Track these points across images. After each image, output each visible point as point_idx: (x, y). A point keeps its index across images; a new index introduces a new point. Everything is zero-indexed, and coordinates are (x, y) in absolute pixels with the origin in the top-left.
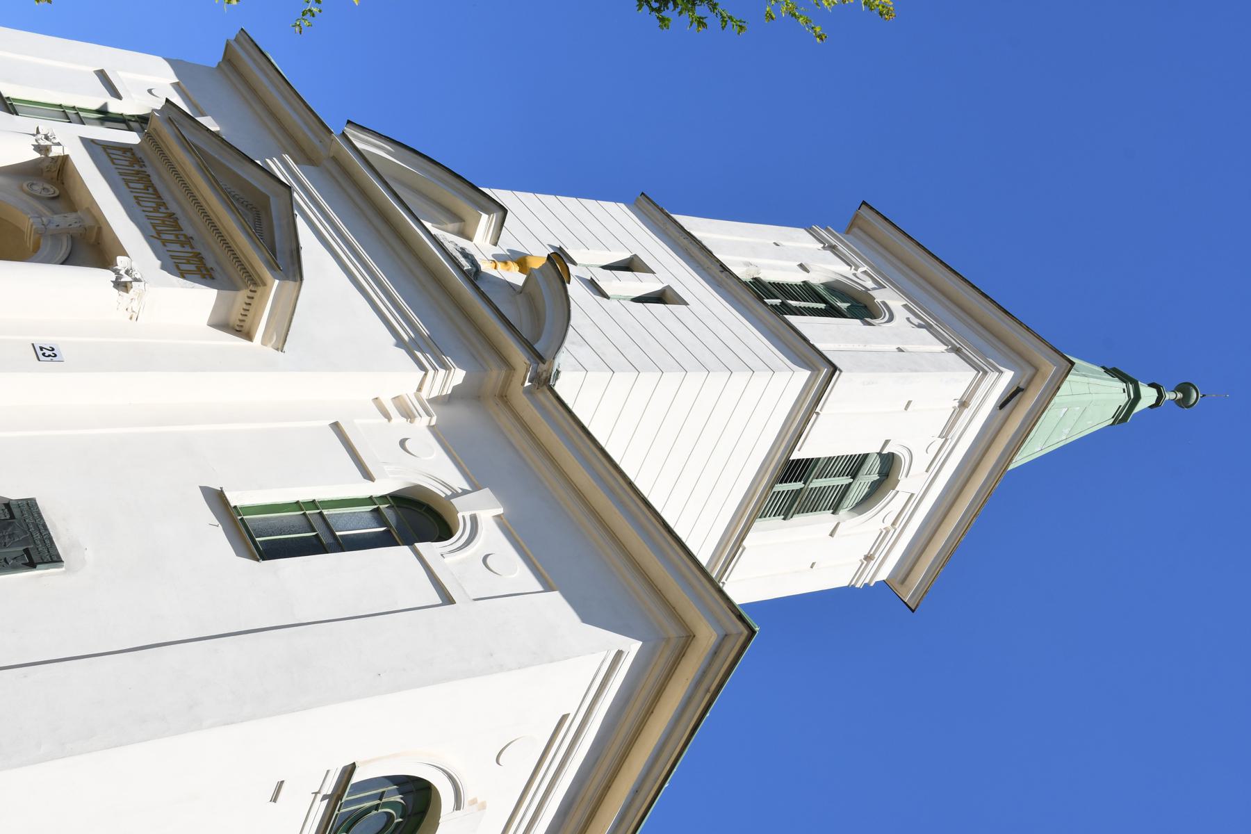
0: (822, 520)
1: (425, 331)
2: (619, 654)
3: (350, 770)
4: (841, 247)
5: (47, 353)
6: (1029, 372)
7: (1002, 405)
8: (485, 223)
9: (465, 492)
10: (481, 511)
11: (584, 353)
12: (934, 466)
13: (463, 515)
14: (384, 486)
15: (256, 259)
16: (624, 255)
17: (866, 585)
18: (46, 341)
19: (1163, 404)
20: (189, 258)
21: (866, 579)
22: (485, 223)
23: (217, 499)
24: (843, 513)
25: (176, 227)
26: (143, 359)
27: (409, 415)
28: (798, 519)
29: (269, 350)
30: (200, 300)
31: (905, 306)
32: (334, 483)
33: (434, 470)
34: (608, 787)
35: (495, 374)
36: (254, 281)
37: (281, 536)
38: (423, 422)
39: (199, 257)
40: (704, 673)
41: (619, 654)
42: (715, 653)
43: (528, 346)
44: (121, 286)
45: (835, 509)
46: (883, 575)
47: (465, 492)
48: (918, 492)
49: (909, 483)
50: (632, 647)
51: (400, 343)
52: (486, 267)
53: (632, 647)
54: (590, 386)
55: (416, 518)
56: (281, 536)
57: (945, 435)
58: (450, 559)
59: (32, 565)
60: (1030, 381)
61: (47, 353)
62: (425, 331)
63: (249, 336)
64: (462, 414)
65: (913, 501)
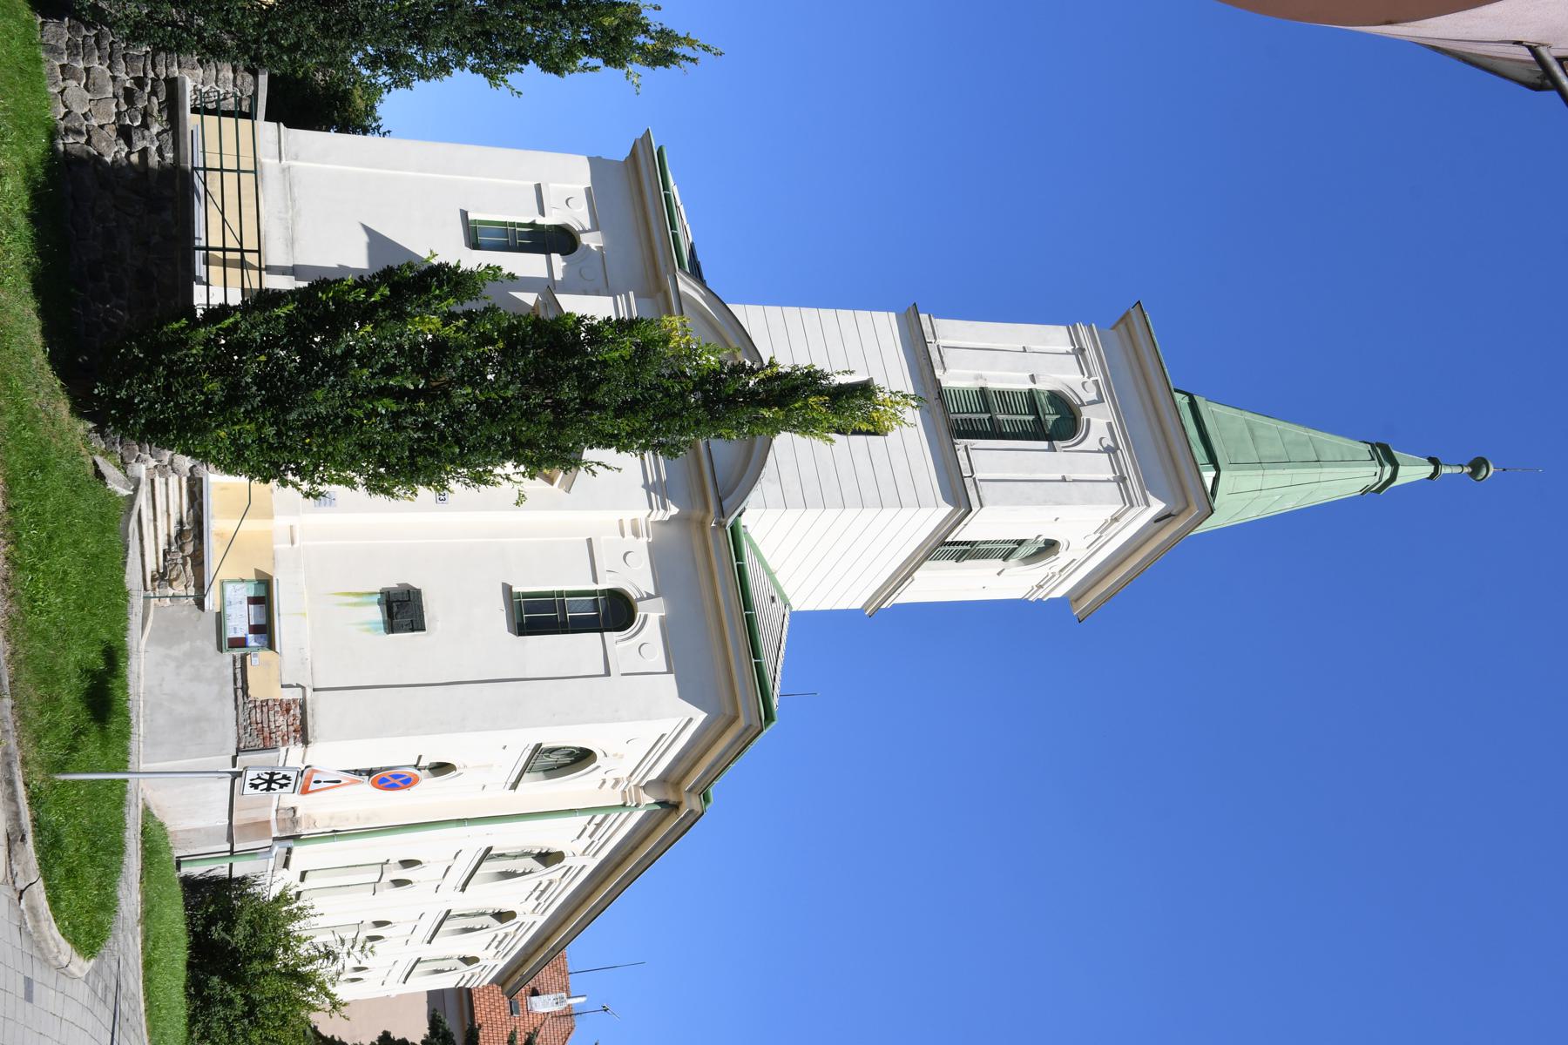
1: (664, 477)
2: (691, 720)
4: (1091, 353)
6: (1180, 506)
7: (1157, 520)
9: (650, 597)
13: (640, 615)
17: (1039, 601)
19: (1437, 479)
21: (1040, 594)
24: (1011, 561)
27: (636, 534)
28: (968, 562)
29: (562, 491)
31: (1110, 425)
33: (636, 578)
34: (701, 757)
35: (698, 513)
38: (644, 540)
40: (741, 735)
41: (691, 720)
42: (746, 729)
43: (720, 501)
44: (662, 57)
45: (1005, 559)
46: (1059, 593)
47: (650, 597)
49: (1063, 557)
50: (700, 716)
51: (646, 486)
53: (700, 716)
55: (614, 612)
56: (537, 616)
58: (621, 645)
59: (413, 630)
62: (664, 477)
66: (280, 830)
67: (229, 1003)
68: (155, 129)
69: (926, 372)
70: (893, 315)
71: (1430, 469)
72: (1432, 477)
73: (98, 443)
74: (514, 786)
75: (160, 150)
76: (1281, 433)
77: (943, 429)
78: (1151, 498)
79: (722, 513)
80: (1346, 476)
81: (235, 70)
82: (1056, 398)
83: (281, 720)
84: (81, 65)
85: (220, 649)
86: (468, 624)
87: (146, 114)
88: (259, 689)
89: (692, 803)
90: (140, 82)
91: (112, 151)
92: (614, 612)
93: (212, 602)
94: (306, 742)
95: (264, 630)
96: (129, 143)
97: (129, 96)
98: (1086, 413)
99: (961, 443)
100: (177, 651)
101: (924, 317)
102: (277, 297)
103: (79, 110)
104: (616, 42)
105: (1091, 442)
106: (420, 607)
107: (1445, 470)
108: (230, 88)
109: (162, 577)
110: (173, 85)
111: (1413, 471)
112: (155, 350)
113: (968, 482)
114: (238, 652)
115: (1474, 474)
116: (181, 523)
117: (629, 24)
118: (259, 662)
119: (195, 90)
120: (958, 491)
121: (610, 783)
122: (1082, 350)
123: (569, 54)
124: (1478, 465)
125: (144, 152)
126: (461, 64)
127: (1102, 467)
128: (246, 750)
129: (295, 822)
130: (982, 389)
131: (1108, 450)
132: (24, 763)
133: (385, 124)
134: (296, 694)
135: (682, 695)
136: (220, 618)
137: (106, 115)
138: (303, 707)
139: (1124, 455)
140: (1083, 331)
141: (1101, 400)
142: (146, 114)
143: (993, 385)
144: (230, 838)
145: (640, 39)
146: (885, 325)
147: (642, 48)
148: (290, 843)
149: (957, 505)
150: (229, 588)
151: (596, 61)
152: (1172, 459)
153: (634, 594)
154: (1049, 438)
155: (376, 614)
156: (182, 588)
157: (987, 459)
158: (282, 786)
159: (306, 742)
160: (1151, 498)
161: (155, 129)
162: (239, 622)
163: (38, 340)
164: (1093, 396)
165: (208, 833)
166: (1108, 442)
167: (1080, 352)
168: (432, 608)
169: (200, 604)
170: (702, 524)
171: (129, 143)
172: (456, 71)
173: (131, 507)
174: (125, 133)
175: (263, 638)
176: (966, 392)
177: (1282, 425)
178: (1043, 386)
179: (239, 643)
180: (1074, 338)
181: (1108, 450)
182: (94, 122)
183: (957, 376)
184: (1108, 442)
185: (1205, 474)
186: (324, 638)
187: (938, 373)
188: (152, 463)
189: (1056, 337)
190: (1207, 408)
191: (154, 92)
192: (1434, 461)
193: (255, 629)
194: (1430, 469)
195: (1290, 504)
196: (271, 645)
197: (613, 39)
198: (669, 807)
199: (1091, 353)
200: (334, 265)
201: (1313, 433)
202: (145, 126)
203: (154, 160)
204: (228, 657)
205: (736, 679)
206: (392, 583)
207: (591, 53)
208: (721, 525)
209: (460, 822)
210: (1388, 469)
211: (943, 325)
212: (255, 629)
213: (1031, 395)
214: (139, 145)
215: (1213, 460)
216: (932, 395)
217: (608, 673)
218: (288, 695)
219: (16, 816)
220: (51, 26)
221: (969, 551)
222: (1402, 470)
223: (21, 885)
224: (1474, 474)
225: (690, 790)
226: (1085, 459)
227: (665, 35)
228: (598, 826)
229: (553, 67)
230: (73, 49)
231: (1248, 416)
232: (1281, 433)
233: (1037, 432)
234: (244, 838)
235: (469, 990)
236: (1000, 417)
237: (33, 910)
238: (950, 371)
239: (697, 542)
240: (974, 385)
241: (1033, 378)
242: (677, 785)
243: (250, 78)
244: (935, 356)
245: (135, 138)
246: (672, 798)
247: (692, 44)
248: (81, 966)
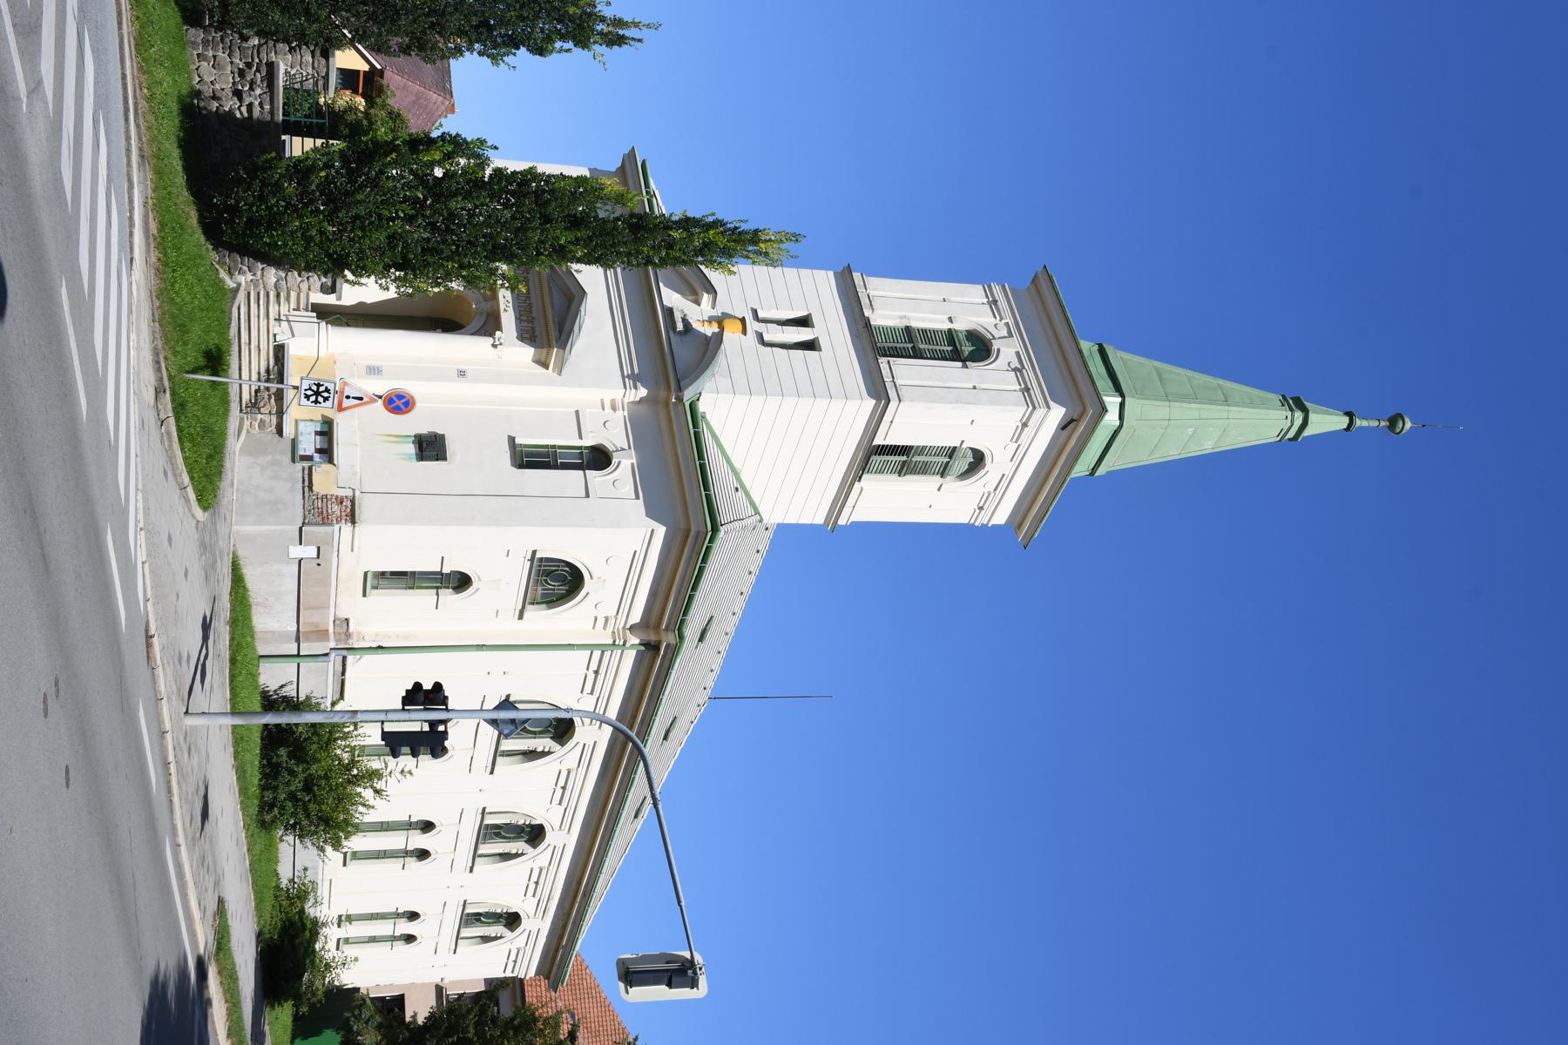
0: (932, 481)
3: (534, 552)
4: (1002, 303)
5: (462, 374)
6: (1079, 410)
8: (706, 298)
10: (1008, 350)
12: (1018, 458)
18: (462, 367)
19: (1353, 429)
20: (528, 335)
21: (983, 519)
22: (706, 298)
23: (512, 440)
25: (530, 312)
26: (498, 377)
27: (614, 409)
30: (528, 352)
31: (1018, 353)
32: (564, 438)
33: (614, 435)
35: (663, 394)
36: (550, 346)
37: (530, 459)
38: (620, 413)
39: (533, 329)
43: (678, 381)
44: (616, 40)
52: (695, 325)
54: (720, 404)
55: (598, 458)
56: (530, 459)
57: (1016, 438)
60: (1081, 415)
61: (462, 374)
63: (546, 367)
64: (643, 409)
66: (337, 640)
67: (292, 773)
68: (258, 91)
69: (857, 309)
70: (831, 273)
71: (1346, 420)
72: (1348, 429)
74: (521, 617)
75: (261, 104)
76: (1189, 378)
77: (869, 348)
78: (1052, 404)
79: (680, 389)
81: (313, 53)
82: (973, 336)
83: (336, 508)
84: (211, 53)
85: (293, 461)
86: (478, 459)
87: (252, 83)
88: (318, 487)
89: (668, 639)
90: (249, 65)
91: (229, 104)
92: (598, 458)
94: (353, 522)
95: (327, 452)
96: (240, 99)
97: (242, 73)
98: (996, 345)
100: (261, 460)
101: (857, 276)
103: (208, 79)
104: (583, 29)
105: (1001, 363)
106: (444, 446)
107: (1359, 423)
108: (310, 70)
109: (254, 405)
110: (271, 67)
111: (1326, 422)
112: (253, 171)
113: (889, 386)
114: (306, 464)
116: (268, 371)
117: (590, 15)
118: (322, 473)
119: (286, 72)
120: (879, 390)
122: (995, 302)
123: (549, 39)
125: (250, 106)
128: (309, 524)
129: (348, 635)
130: (908, 328)
131: (1015, 370)
132: (166, 358)
133: (531, 612)
134: (349, 493)
135: (648, 515)
136: (294, 443)
137: (225, 83)
138: (353, 502)
139: (1029, 373)
140: (997, 290)
141: (1010, 335)
142: (252, 83)
143: (915, 324)
144: (298, 640)
145: (599, 27)
146: (825, 281)
148: (345, 653)
150: (301, 425)
151: (570, 45)
152: (1074, 380)
153: (611, 448)
154: (964, 361)
155: (411, 449)
156: (267, 416)
157: (904, 371)
158: (326, 399)
159: (353, 522)
160: (1052, 404)
161: (258, 91)
162: (308, 445)
163: (180, 168)
164: (1004, 332)
166: (1015, 364)
167: (993, 303)
168: (451, 447)
170: (667, 403)
171: (240, 99)
172: (467, 54)
173: (234, 298)
174: (238, 94)
175: (325, 457)
176: (893, 330)
177: (1190, 373)
178: (961, 326)
180: (989, 292)
181: (1015, 370)
182: (217, 86)
184: (1015, 364)
186: (368, 450)
187: (867, 313)
189: (975, 293)
190: (1117, 357)
191: (258, 70)
192: (1350, 414)
193: (319, 451)
196: (331, 461)
197: (580, 26)
198: (651, 648)
199: (1002, 303)
201: (1221, 382)
202: (252, 89)
204: (299, 466)
205: (689, 500)
206: (424, 430)
207: (563, 38)
208: (680, 400)
209: (480, 647)
210: (1299, 416)
211: (872, 282)
212: (319, 451)
214: (247, 100)
215: (1118, 389)
216: (861, 328)
217: (587, 496)
218: (341, 493)
219: (161, 379)
220: (192, 31)
221: (905, 459)
222: (1312, 417)
223: (163, 416)
225: (667, 629)
226: (996, 375)
227: (619, 23)
228: (596, 672)
229: (540, 51)
231: (1157, 364)
232: (1189, 378)
233: (956, 355)
234: (308, 639)
235: (521, 980)
236: (922, 346)
237: (169, 433)
238: (879, 312)
239: (662, 416)
241: (950, 319)
243: (323, 61)
245: (235, 445)
246: (653, 638)
247: (636, 25)
248: (198, 512)
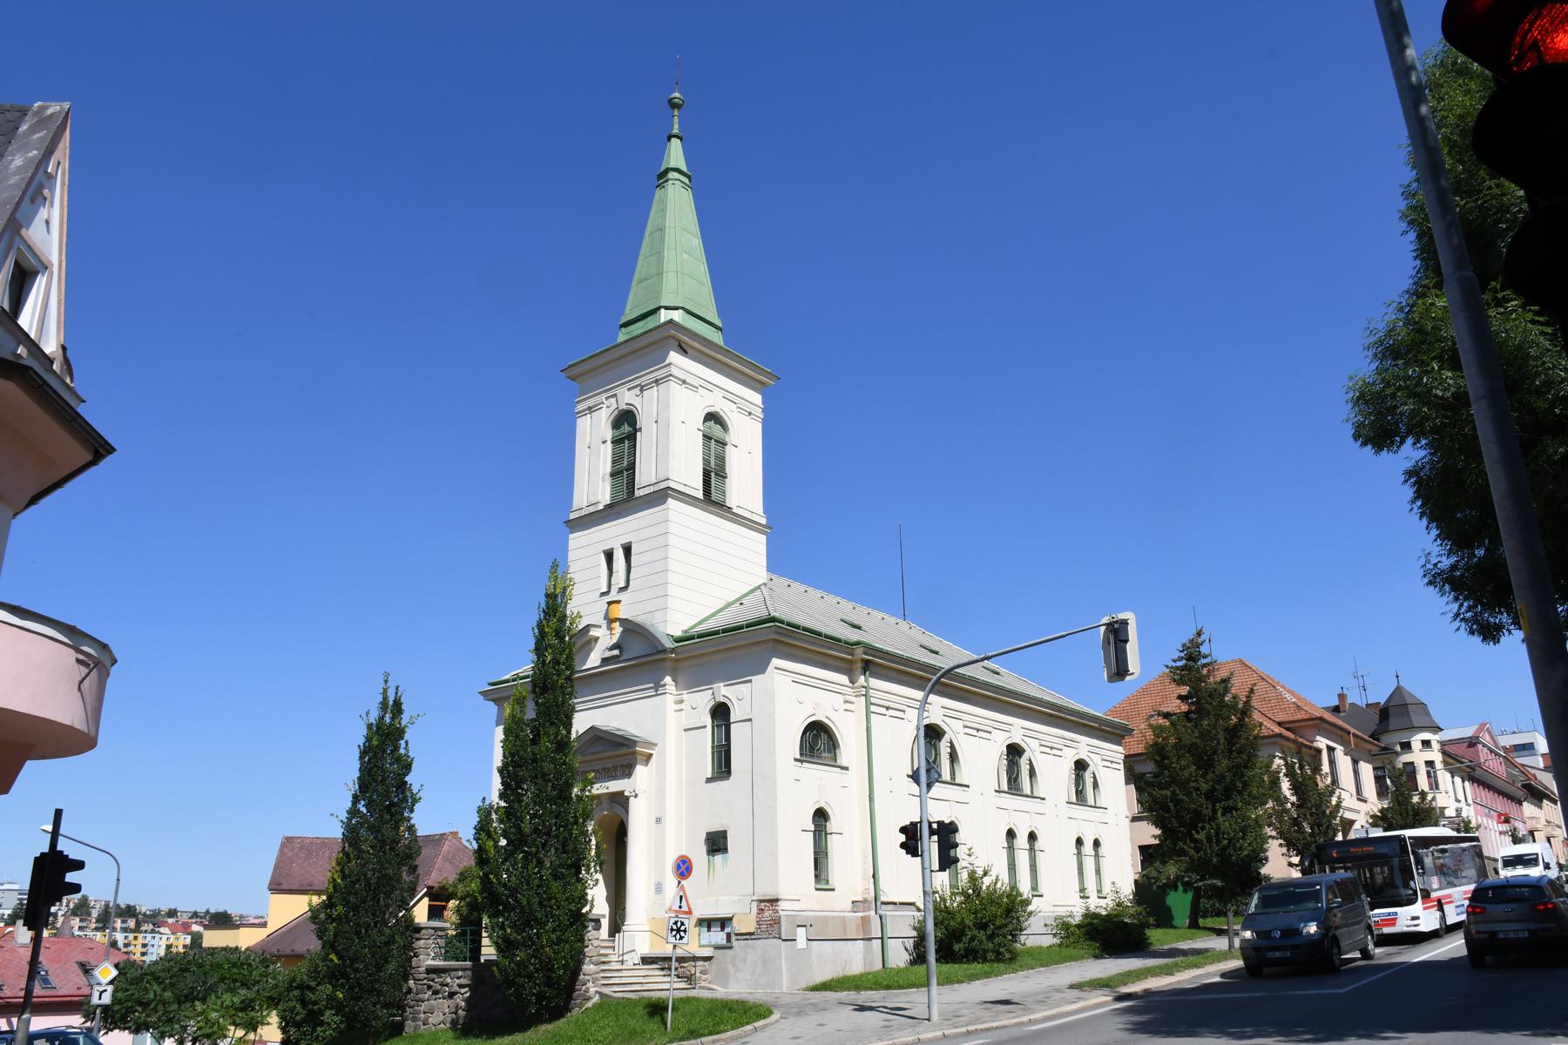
4: (590, 403)
5: (658, 820)
11: (658, 617)
12: (710, 386)
14: (708, 721)
15: (624, 750)
16: (603, 558)
20: (626, 770)
21: (758, 412)
22: (593, 633)
23: (709, 780)
26: (661, 793)
32: (706, 739)
35: (668, 664)
36: (635, 753)
37: (723, 765)
38: (685, 697)
44: (397, 708)
48: (720, 393)
52: (615, 640)
55: (721, 713)
56: (723, 765)
61: (658, 820)
65: (729, 397)
67: (973, 939)
71: (675, 142)
73: (576, 1011)
74: (846, 769)
79: (665, 651)
80: (677, 208)
86: (724, 806)
87: (443, 985)
88: (750, 926)
90: (429, 987)
91: (459, 1000)
92: (721, 713)
93: (707, 952)
95: (724, 922)
97: (436, 993)
98: (623, 407)
99: (638, 493)
101: (572, 516)
102: (1317, 769)
103: (441, 1018)
105: (636, 402)
107: (676, 131)
109: (689, 978)
110: (430, 971)
111: (676, 155)
115: (677, 106)
118: (740, 926)
120: (661, 496)
121: (848, 706)
123: (398, 759)
124: (673, 105)
125: (460, 986)
126: (409, 819)
127: (652, 393)
129: (865, 901)
135: (763, 672)
136: (717, 948)
137: (444, 1005)
138: (761, 901)
139: (644, 380)
140: (580, 407)
142: (443, 985)
143: (609, 470)
145: (388, 719)
147: (393, 719)
149: (667, 496)
151: (402, 742)
152: (649, 345)
153: (712, 703)
154: (636, 431)
155: (718, 858)
157: (645, 477)
162: (718, 937)
164: (613, 400)
165: (868, 953)
166: (637, 391)
169: (708, 959)
170: (676, 660)
174: (452, 995)
176: (613, 487)
178: (608, 434)
179: (729, 935)
180: (582, 413)
183: (603, 494)
184: (637, 391)
185: (662, 320)
186: (721, 891)
187: (601, 507)
188: (590, 984)
189: (584, 425)
194: (675, 142)
195: (696, 242)
196: (730, 919)
199: (590, 403)
200: (1524, 646)
203: (463, 981)
204: (734, 943)
206: (704, 849)
208: (673, 650)
211: (576, 504)
213: (616, 442)
218: (755, 910)
221: (713, 474)
222: (672, 165)
224: (677, 106)
226: (646, 405)
227: (384, 705)
229: (408, 767)
230: (415, 1019)
233: (632, 437)
240: (608, 481)
242: (851, 662)
244: (592, 509)
246: (859, 665)
